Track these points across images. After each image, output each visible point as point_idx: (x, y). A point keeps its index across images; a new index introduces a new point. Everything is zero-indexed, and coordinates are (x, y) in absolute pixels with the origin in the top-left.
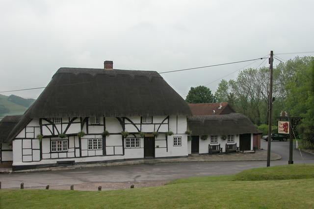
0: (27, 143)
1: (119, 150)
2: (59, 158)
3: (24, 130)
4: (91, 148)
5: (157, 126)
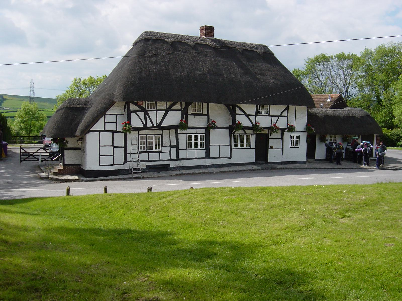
0: (106, 138)
1: (225, 151)
2: (149, 161)
4: (191, 147)
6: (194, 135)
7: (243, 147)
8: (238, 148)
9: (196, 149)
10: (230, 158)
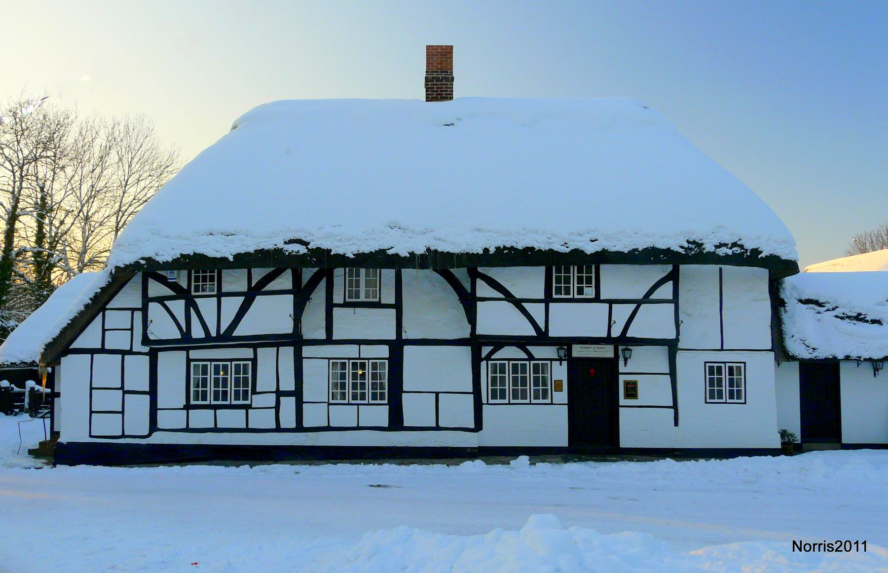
0: (108, 366)
3: (100, 317)
5: (622, 313)
6: (352, 363)
9: (359, 402)
10: (478, 426)
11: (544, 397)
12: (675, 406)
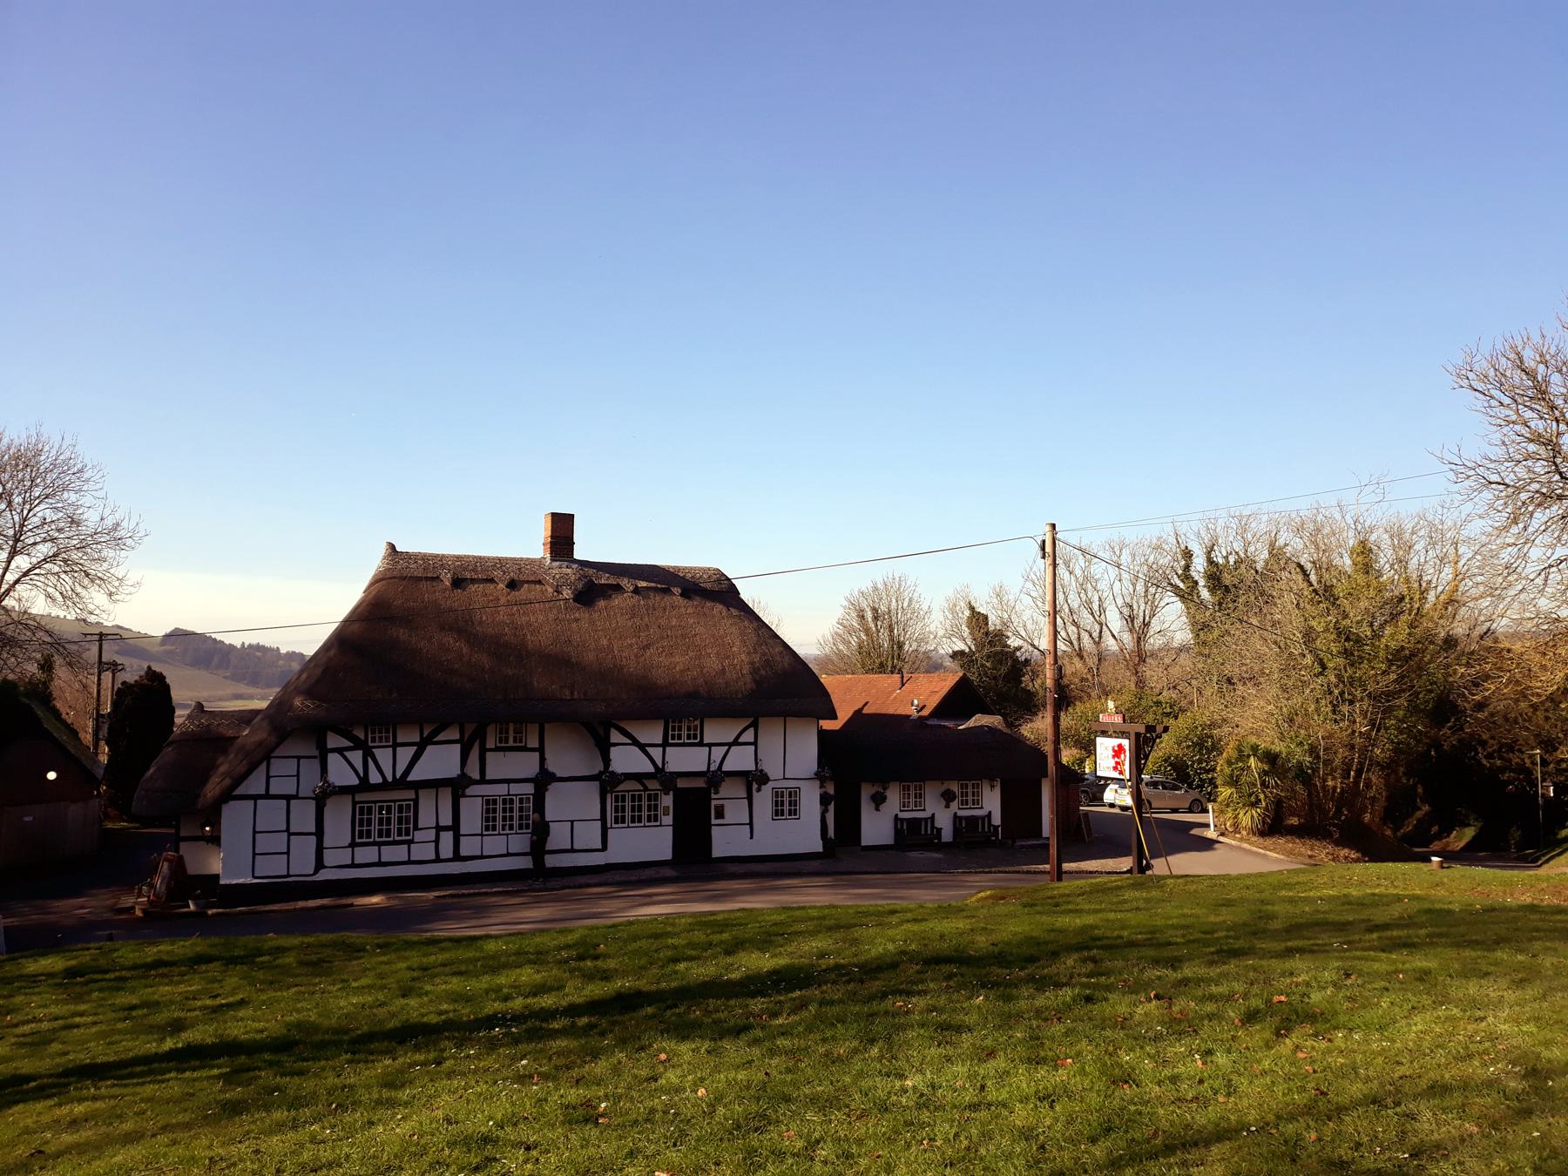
0: (271, 814)
1: (589, 835)
5: (718, 753)
7: (640, 821)
8: (626, 825)
10: (604, 848)
11: (656, 820)
12: (751, 824)
